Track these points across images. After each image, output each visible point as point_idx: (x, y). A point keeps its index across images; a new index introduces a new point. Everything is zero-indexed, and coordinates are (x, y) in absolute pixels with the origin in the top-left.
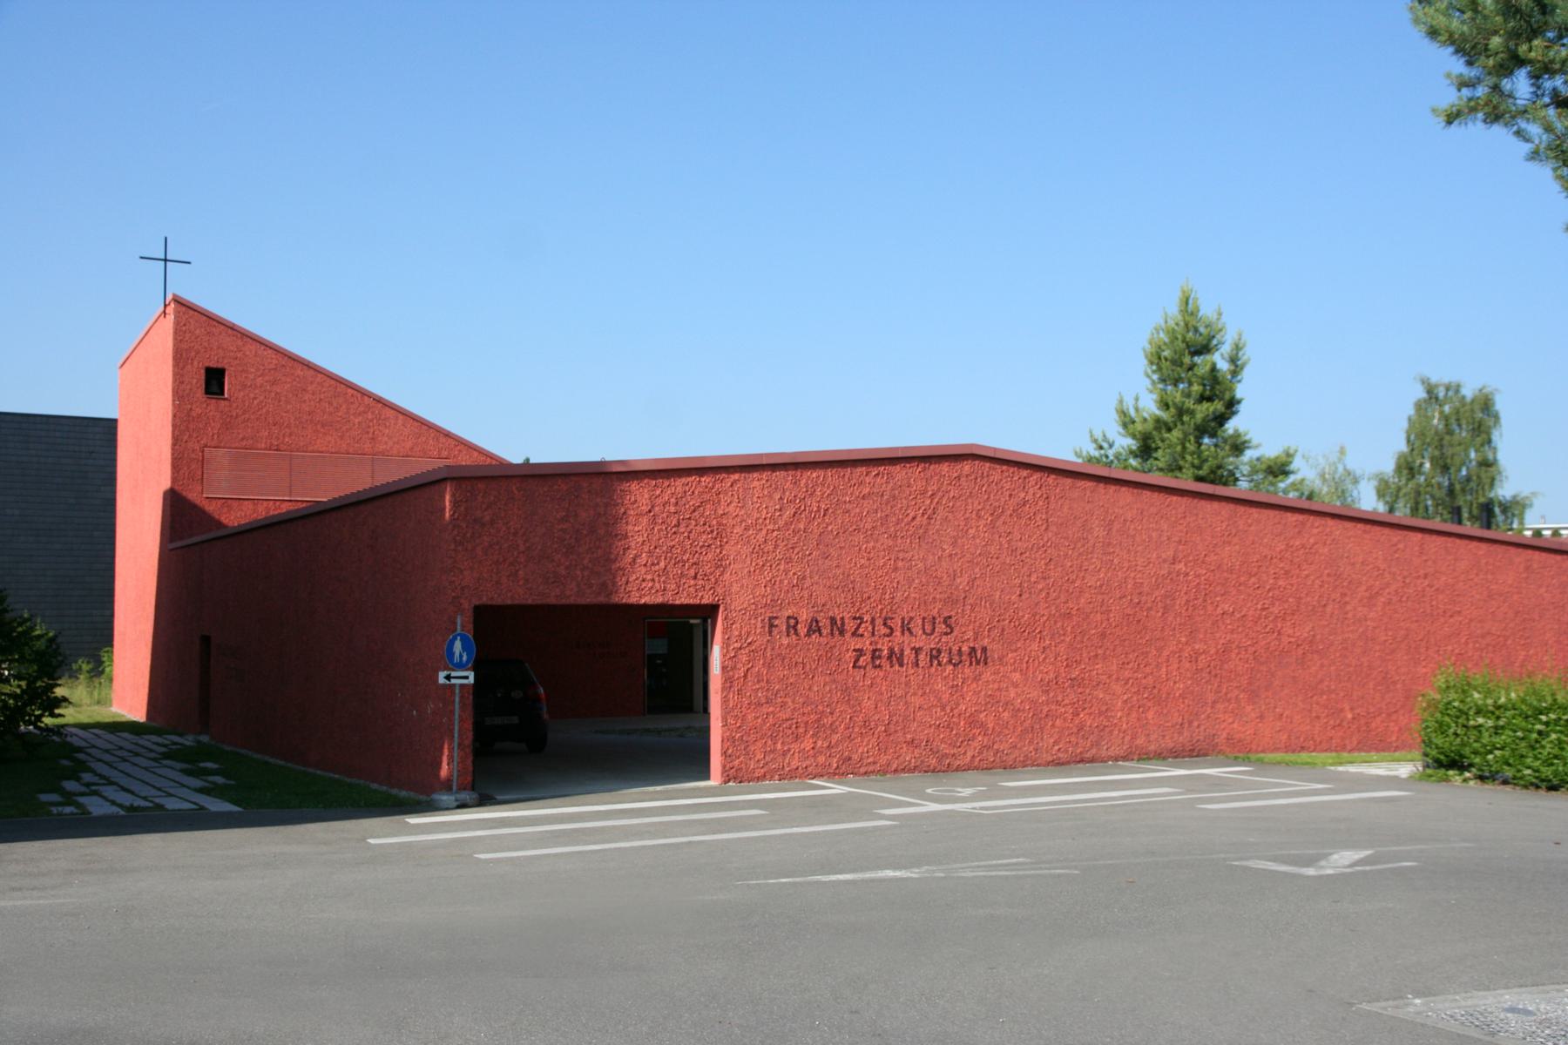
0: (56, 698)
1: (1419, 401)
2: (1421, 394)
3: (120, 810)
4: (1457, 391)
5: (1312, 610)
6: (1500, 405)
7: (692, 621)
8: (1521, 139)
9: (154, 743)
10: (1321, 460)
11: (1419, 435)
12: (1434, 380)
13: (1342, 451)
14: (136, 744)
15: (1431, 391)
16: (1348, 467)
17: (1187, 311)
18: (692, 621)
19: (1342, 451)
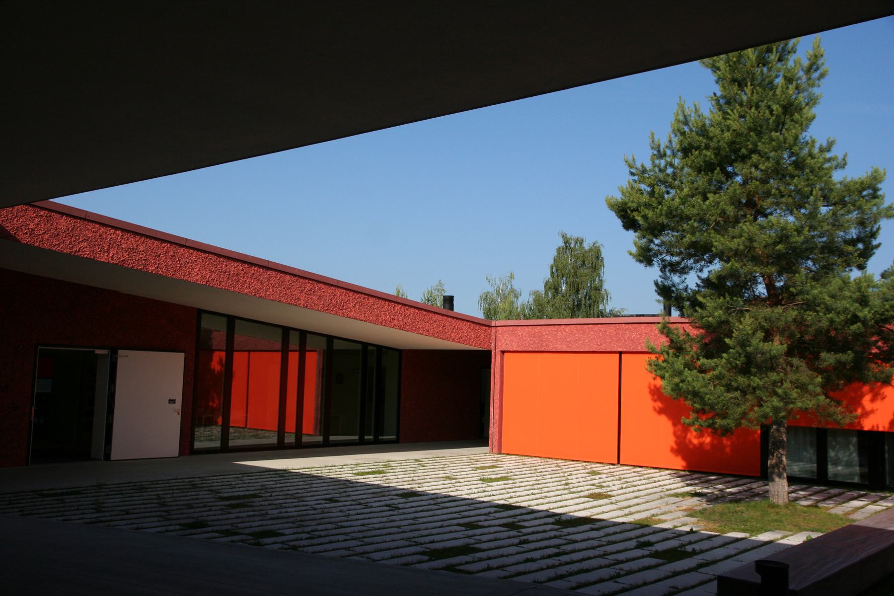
0: (296, 442)
1: (559, 248)
2: (561, 243)
3: (762, 47)
4: (581, 243)
5: (771, 226)
6: (604, 254)
7: (98, 352)
8: (545, 556)
9: (51, 500)
10: (498, 282)
11: (558, 270)
12: (569, 236)
13: (512, 276)
14: (86, 493)
15: (567, 241)
16: (515, 287)
17: (820, 223)
18: (98, 352)
19: (512, 276)
